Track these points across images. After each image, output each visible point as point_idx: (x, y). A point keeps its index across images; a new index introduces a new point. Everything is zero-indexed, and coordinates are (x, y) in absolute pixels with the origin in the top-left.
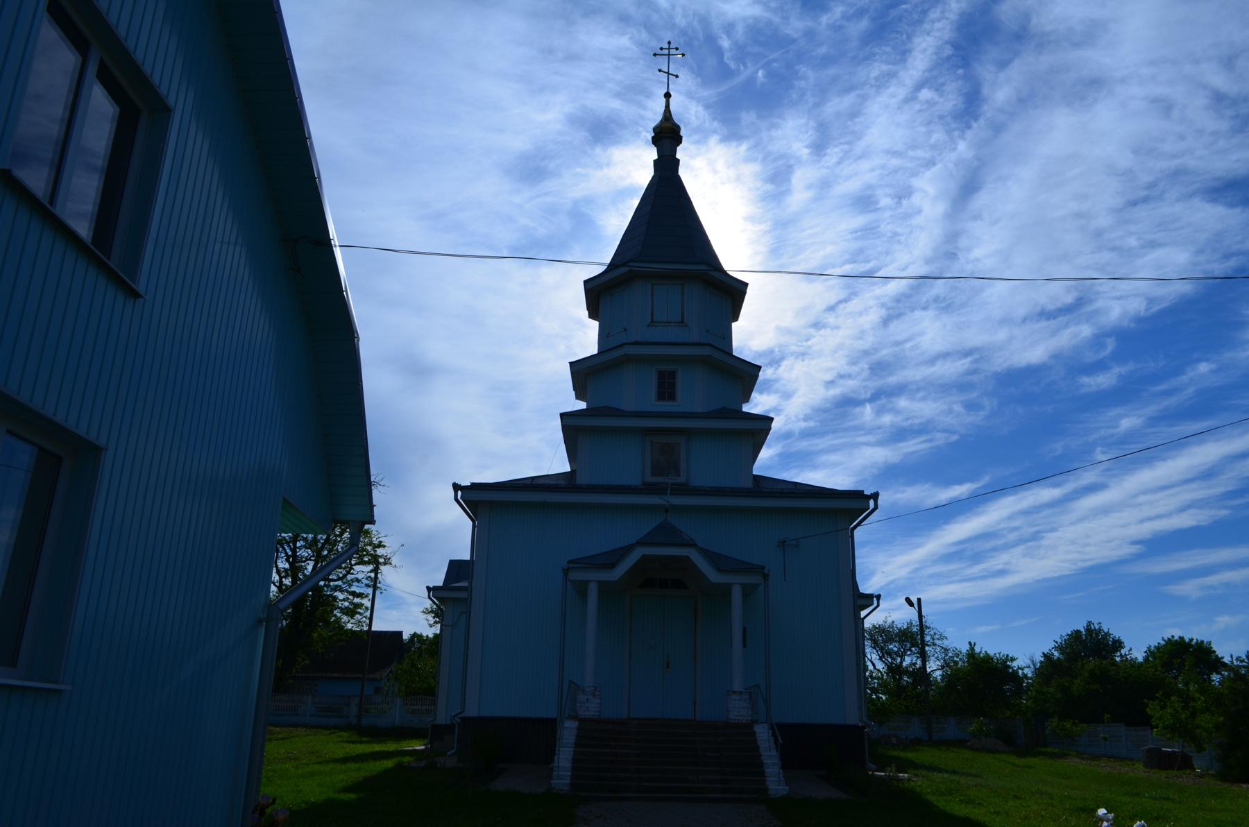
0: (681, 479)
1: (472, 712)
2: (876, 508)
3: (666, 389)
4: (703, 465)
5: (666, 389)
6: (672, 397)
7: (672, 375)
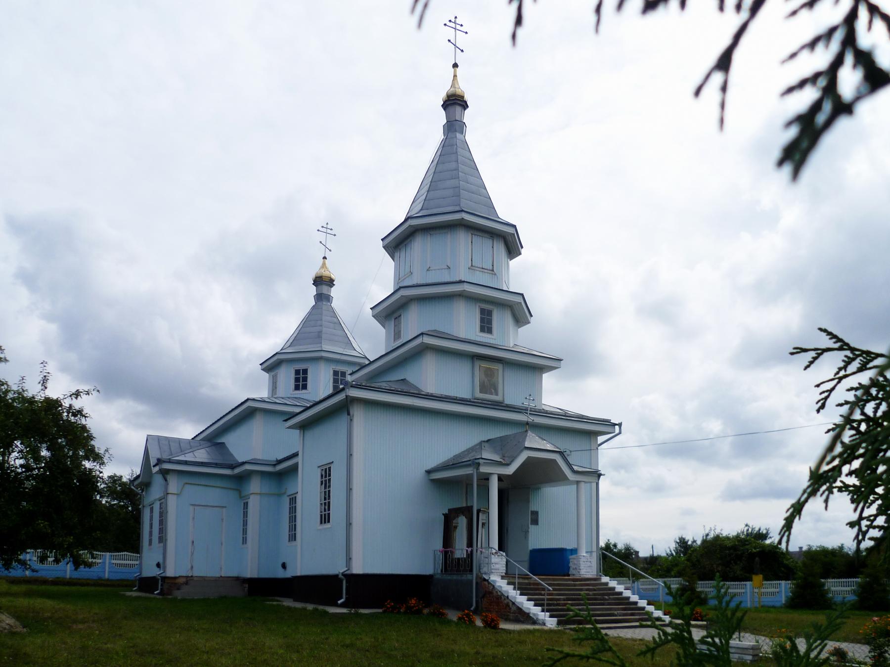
0: (498, 398)
1: (358, 568)
2: (620, 433)
3: (486, 326)
4: (512, 390)
5: (486, 326)
6: (490, 331)
7: (490, 313)
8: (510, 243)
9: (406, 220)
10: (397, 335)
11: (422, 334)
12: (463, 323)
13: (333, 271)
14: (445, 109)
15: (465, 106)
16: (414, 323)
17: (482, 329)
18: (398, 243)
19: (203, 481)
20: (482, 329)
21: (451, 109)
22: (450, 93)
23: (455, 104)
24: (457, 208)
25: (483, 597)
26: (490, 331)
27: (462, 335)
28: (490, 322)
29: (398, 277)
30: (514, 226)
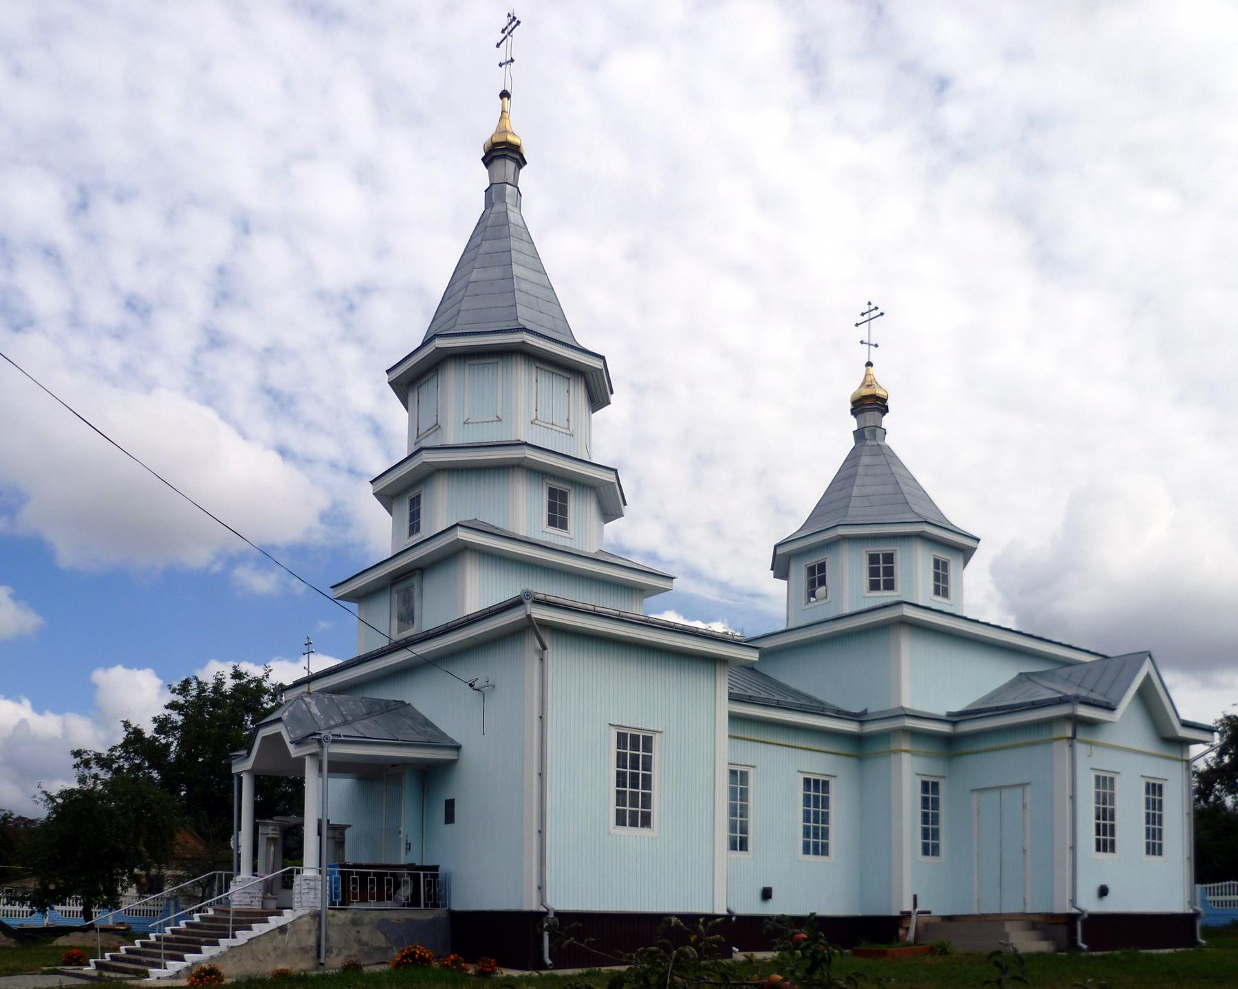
3: (558, 517)
5: (558, 517)
6: (563, 525)
7: (564, 496)
8: (594, 385)
9: (424, 344)
10: (414, 527)
11: (457, 525)
12: (522, 511)
13: (886, 384)
14: (487, 165)
15: (521, 162)
16: (445, 508)
17: (552, 522)
18: (410, 380)
19: (1009, 741)
20: (552, 522)
21: (498, 164)
22: (496, 140)
23: (504, 156)
24: (513, 325)
25: (932, 950)
26: (563, 525)
27: (522, 532)
28: (564, 511)
29: (417, 432)
30: (603, 358)
